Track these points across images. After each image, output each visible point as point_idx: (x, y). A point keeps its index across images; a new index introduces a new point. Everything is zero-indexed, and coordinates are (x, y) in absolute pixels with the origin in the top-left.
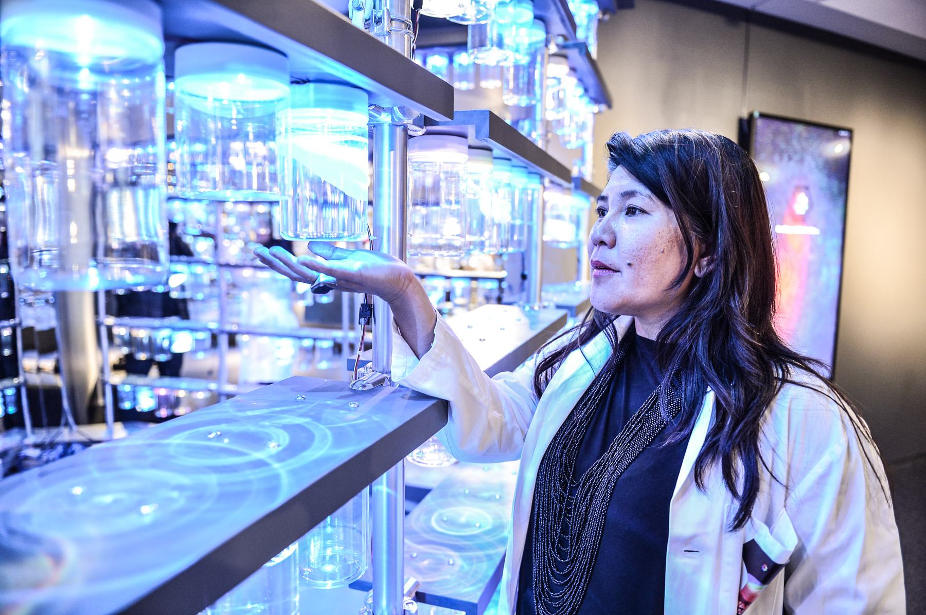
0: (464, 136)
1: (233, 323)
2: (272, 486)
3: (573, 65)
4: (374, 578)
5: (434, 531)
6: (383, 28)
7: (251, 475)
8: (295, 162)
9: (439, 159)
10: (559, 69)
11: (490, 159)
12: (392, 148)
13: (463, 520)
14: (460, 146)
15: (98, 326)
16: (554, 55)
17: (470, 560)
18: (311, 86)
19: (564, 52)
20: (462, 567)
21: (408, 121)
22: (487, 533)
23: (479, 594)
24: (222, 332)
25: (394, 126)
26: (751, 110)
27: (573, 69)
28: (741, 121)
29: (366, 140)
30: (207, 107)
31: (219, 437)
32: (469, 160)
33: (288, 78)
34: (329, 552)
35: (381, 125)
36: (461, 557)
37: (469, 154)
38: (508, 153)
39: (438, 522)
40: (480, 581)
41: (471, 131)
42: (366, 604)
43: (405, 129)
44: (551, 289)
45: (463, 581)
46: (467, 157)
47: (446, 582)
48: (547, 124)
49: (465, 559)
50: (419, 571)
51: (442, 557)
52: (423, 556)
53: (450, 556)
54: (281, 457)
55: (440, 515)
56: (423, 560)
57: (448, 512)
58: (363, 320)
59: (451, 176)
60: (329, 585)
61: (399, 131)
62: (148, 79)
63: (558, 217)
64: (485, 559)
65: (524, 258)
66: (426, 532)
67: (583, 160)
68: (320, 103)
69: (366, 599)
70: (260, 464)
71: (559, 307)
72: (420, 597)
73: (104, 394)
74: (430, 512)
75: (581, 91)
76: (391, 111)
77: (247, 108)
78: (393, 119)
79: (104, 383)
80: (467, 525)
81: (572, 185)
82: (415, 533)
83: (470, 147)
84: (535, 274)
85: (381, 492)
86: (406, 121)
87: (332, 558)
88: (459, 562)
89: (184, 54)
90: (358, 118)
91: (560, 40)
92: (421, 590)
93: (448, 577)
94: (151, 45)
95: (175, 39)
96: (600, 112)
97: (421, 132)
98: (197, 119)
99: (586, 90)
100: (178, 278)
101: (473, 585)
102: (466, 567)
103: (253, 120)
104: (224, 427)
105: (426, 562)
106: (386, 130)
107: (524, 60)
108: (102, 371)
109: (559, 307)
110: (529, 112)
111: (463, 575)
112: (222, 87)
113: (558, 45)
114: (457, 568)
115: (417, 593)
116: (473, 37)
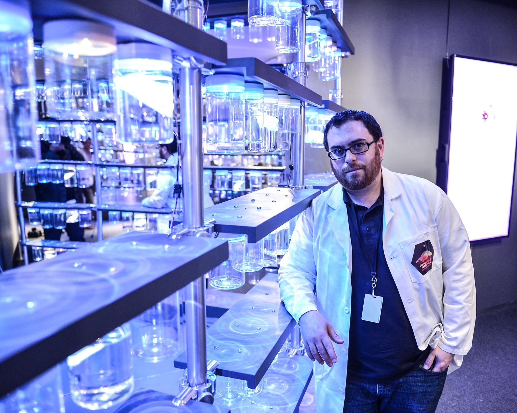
0: (242, 75)
1: (106, 205)
2: (109, 291)
3: (323, 24)
4: (188, 361)
5: (230, 332)
6: (183, 5)
7: (97, 286)
8: (124, 93)
9: (227, 90)
10: (314, 28)
11: (262, 90)
12: (191, 83)
13: (250, 325)
14: (239, 82)
15: (17, 207)
16: (309, 19)
17: (252, 350)
18: (133, 45)
19: (317, 16)
20: (247, 354)
21: (201, 66)
22: (265, 333)
23: (256, 370)
24: (99, 210)
25: (192, 69)
26: (451, 54)
27: (324, 28)
28: (445, 60)
29: (170, 79)
30: (65, 59)
31: (80, 267)
32: (245, 90)
33: (114, 40)
34: (155, 341)
35: (184, 68)
36: (246, 347)
37: (245, 87)
38: (271, 85)
39: (232, 327)
40: (258, 362)
41: (244, 70)
42: (184, 376)
43: (200, 71)
44: (313, 176)
45: (246, 362)
46: (244, 88)
47: (236, 362)
48: (307, 66)
49: (248, 349)
50: (219, 356)
51: (235, 348)
52: (222, 347)
53: (240, 347)
54: (117, 276)
55: (235, 322)
56: (223, 349)
57: (239, 321)
58: (176, 195)
59: (237, 101)
60: (155, 360)
61: (196, 72)
62: (21, 44)
63: (315, 128)
64: (261, 349)
65: (290, 155)
66: (225, 333)
67: (335, 88)
68: (139, 55)
69: (184, 373)
70: (103, 280)
71: (315, 187)
72: (218, 372)
73: (23, 252)
74: (229, 321)
75: (330, 43)
76: (188, 59)
77: (90, 60)
78: (191, 65)
79: (23, 245)
80: (252, 328)
81: (323, 106)
82: (219, 333)
83: (246, 82)
84: (300, 167)
85: (190, 304)
86: (199, 66)
87: (158, 344)
88: (245, 350)
89: (49, 28)
90: (166, 65)
91: (314, 9)
92: (219, 368)
93: (237, 360)
94: (23, 23)
95: (39, 20)
96: (346, 56)
97: (212, 72)
98: (58, 67)
99: (335, 42)
100: (70, 173)
101: (252, 364)
102: (249, 354)
103: (95, 67)
104: (84, 260)
105: (224, 351)
106: (187, 71)
107: (289, 23)
108: (21, 237)
109: (315, 187)
110: (293, 58)
111: (247, 358)
112: (75, 47)
113: (311, 12)
114: (243, 354)
115: (217, 370)
116: (251, 8)
